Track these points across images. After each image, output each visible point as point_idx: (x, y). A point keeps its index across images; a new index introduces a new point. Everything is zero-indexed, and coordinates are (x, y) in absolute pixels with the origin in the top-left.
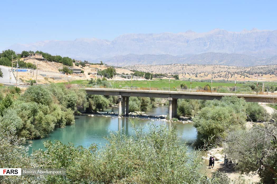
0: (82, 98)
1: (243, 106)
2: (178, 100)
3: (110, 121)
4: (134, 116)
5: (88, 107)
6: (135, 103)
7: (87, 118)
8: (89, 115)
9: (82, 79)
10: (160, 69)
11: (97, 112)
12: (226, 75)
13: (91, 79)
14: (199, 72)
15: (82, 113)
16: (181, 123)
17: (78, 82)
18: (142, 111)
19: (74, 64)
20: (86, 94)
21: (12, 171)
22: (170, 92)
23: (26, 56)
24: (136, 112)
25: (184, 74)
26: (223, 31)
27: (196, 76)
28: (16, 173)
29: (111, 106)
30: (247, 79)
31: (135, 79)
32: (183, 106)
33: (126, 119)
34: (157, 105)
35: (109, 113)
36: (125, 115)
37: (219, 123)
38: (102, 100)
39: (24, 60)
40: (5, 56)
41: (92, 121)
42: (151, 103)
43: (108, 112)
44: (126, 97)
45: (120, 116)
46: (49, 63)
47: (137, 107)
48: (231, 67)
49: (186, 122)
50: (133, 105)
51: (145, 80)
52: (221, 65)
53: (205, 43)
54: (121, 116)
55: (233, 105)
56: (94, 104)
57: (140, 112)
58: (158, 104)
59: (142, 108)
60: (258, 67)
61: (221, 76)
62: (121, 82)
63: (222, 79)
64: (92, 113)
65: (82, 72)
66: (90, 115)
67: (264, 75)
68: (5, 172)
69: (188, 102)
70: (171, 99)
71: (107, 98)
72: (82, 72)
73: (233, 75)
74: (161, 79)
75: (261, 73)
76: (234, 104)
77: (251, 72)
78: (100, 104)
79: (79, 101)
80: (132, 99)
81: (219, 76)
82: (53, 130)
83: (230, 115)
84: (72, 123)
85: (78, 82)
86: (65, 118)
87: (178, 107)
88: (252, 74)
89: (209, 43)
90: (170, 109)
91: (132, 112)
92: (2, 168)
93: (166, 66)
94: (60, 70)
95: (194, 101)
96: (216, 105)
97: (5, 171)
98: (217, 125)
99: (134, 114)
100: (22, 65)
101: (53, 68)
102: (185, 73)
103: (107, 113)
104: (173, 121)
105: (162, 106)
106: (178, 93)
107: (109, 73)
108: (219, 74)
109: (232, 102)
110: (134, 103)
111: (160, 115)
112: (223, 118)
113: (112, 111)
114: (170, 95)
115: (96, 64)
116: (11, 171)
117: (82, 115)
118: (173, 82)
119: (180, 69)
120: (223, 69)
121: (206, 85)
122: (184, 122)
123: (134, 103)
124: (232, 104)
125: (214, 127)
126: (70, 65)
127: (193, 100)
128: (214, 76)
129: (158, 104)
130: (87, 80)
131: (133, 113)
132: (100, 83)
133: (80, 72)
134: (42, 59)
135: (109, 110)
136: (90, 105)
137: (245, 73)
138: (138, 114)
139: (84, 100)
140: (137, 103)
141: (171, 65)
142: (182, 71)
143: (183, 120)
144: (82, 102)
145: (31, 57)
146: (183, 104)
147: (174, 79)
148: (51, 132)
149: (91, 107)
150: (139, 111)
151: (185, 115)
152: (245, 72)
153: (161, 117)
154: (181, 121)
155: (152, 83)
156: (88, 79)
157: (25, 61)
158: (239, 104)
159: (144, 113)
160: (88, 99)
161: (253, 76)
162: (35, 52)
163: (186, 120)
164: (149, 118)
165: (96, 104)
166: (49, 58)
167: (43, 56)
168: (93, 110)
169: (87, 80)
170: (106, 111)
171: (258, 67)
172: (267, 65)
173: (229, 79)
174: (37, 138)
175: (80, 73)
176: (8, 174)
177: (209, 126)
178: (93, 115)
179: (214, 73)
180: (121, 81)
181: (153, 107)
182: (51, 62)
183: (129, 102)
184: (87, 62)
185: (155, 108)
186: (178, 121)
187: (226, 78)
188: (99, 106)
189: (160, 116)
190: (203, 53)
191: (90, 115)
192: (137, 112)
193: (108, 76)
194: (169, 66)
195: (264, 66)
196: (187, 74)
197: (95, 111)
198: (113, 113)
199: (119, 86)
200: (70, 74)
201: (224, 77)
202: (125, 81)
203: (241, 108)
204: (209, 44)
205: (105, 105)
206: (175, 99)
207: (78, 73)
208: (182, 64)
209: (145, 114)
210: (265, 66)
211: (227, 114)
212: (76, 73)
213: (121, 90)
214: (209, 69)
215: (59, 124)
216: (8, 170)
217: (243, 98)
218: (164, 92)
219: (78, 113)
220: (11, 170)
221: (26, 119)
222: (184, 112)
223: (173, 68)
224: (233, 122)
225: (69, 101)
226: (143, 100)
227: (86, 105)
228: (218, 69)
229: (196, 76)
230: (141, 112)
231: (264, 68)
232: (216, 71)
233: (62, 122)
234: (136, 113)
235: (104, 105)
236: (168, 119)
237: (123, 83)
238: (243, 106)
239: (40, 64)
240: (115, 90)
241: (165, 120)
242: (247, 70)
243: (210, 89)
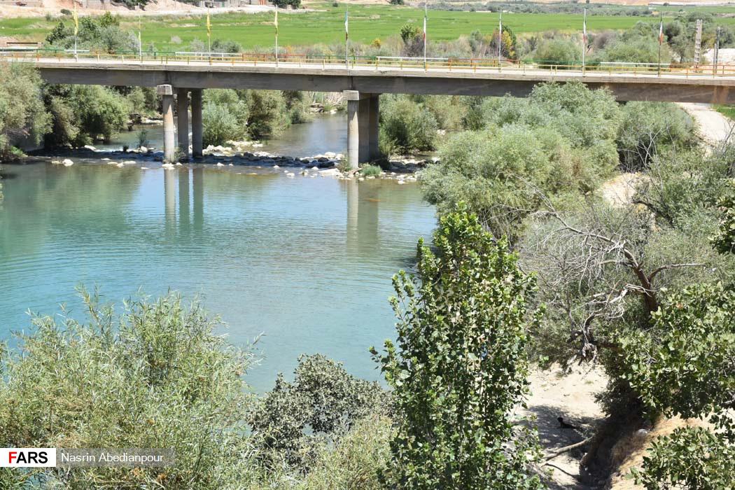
0: (23, 97)
1: (607, 118)
2: (381, 96)
3: (136, 181)
4: (223, 160)
5: (51, 130)
6: (227, 111)
7: (47, 172)
8: (56, 162)
11: (86, 146)
13: (63, 11)
15: (29, 153)
16: (393, 180)
17: (10, 26)
18: (254, 139)
20: (41, 82)
21: (32, 457)
22: (350, 68)
24: (230, 142)
28: (43, 460)
29: (138, 122)
31: (235, 9)
32: (402, 118)
33: (194, 171)
34: (308, 114)
35: (128, 150)
36: (187, 157)
37: (509, 187)
38: (101, 103)
41: (63, 182)
42: (289, 106)
43: (125, 148)
44: (190, 89)
45: (170, 162)
47: (235, 127)
49: (410, 177)
50: (219, 117)
54: (174, 163)
55: (571, 115)
56: (72, 118)
57: (245, 143)
58: (316, 110)
59: (255, 127)
62: (181, 20)
64: (65, 153)
66: (58, 162)
69: (418, 101)
70: (356, 95)
71: (121, 93)
76: (572, 111)
78: (97, 116)
79: (12, 112)
80: (215, 97)
83: (546, 159)
85: (10, 26)
87: (381, 121)
90: (352, 133)
91: (216, 146)
92: (6, 446)
95: (442, 102)
96: (509, 118)
97: (13, 455)
98: (501, 195)
99: (223, 151)
103: (122, 150)
104: (364, 176)
105: (329, 115)
106: (379, 74)
109: (567, 105)
110: (220, 110)
111: (317, 153)
112: (522, 171)
113: (142, 142)
114: (352, 81)
116: (29, 455)
117: (29, 162)
118: (378, 17)
122: (401, 178)
123: (224, 109)
124: (565, 112)
125: (490, 201)
127: (438, 96)
129: (316, 110)
130: (48, 18)
131: (220, 147)
132: (91, 35)
135: (131, 141)
136: (58, 124)
138: (240, 150)
139: (31, 105)
140: (234, 109)
143: (401, 169)
144: (24, 116)
146: (402, 110)
149: (63, 129)
150: (242, 140)
151: (412, 149)
153: (321, 160)
154: (393, 173)
155: (300, 22)
156: (52, 14)
158: (592, 113)
159: (261, 145)
160: (47, 101)
163: (411, 172)
164: (276, 167)
165: (82, 117)
168: (71, 141)
169: (48, 18)
170: (118, 144)
176: (22, 463)
177: (475, 199)
178: (68, 162)
180: (179, 17)
181: (297, 120)
183: (204, 106)
185: (302, 125)
186: (382, 173)
188: (94, 124)
189: (320, 156)
191: (58, 162)
192: (235, 143)
197: (79, 142)
198: (144, 149)
199: (169, 39)
202: (194, 19)
203: (598, 126)
205: (116, 120)
206: (368, 96)
209: (264, 149)
211: (538, 154)
213: (172, 64)
216: (22, 454)
217: (607, 87)
218: (326, 71)
219: (14, 155)
220: (30, 453)
222: (405, 139)
224: (556, 184)
226: (257, 99)
227: (42, 124)
230: (252, 142)
234: (230, 149)
235: (110, 121)
236: (344, 167)
237: (188, 25)
238: (606, 119)
240: (148, 66)
241: (333, 172)
243: (514, 43)
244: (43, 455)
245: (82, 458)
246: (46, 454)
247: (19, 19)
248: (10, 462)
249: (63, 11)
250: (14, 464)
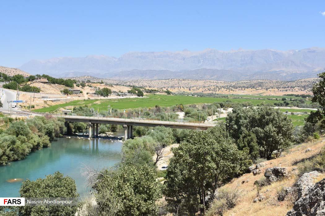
9: (80, 99)
10: (159, 83)
12: (214, 89)
13: (88, 98)
14: (192, 86)
19: (75, 85)
21: (14, 201)
23: (33, 80)
25: (180, 88)
26: (214, 50)
27: (190, 90)
28: (19, 203)
30: (231, 92)
39: (31, 83)
40: (15, 80)
46: (53, 85)
48: (220, 82)
51: (136, 98)
52: (212, 79)
53: (199, 60)
60: (242, 81)
61: (211, 89)
63: (211, 92)
65: (81, 92)
67: (246, 89)
68: (5, 202)
72: (81, 92)
73: (220, 89)
74: (155, 95)
75: (244, 87)
77: (236, 86)
81: (209, 89)
82: (28, 154)
84: (49, 145)
86: (42, 143)
88: (236, 88)
89: (202, 60)
93: (164, 81)
94: (61, 92)
97: (6, 201)
100: (27, 89)
101: (55, 90)
102: (180, 87)
107: (105, 92)
108: (208, 88)
115: (97, 83)
116: (13, 201)
119: (176, 83)
120: (212, 84)
121: (180, 104)
126: (71, 86)
128: (204, 90)
132: (81, 110)
133: (80, 92)
134: (46, 82)
137: (230, 87)
141: (168, 79)
142: (178, 85)
145: (37, 81)
147: (166, 94)
148: (27, 155)
152: (230, 86)
157: (30, 86)
161: (237, 90)
162: (41, 75)
166: (53, 81)
167: (48, 80)
171: (242, 81)
172: (250, 80)
173: (216, 93)
174: (15, 160)
175: (80, 93)
176: (10, 205)
179: (204, 87)
180: (115, 99)
182: (55, 84)
184: (90, 81)
187: (214, 91)
190: (196, 69)
193: (104, 95)
194: (167, 81)
195: (247, 81)
196: (182, 88)
200: (70, 95)
201: (213, 91)
204: (203, 61)
207: (78, 93)
208: (178, 79)
210: (248, 81)
212: (76, 93)
214: (201, 83)
215: (35, 149)
216: (10, 200)
220: (13, 200)
221: (6, 148)
223: (170, 83)
225: (47, 129)
228: (209, 83)
229: (190, 90)
231: (247, 83)
232: (206, 85)
233: (40, 146)
237: (116, 101)
239: (44, 87)
242: (233, 85)
243: (183, 108)
244: (19, 200)
245: (36, 202)
246: (20, 200)
247: (78, 100)
248: (5, 204)
249: (88, 98)
250: (6, 204)
